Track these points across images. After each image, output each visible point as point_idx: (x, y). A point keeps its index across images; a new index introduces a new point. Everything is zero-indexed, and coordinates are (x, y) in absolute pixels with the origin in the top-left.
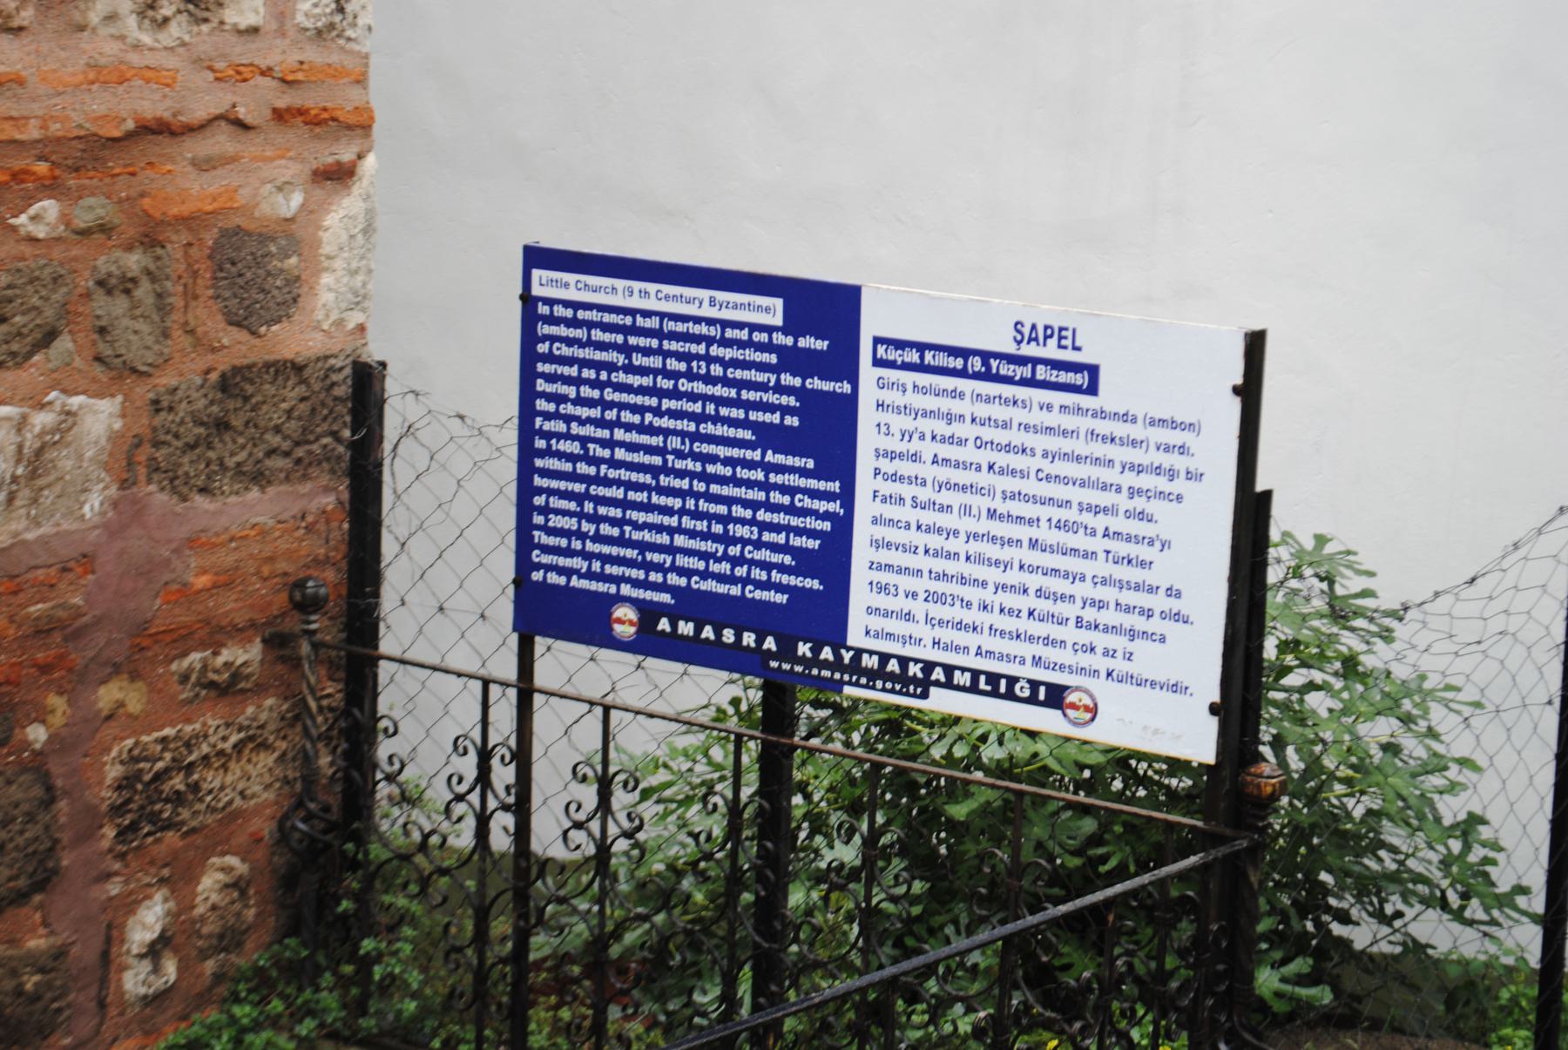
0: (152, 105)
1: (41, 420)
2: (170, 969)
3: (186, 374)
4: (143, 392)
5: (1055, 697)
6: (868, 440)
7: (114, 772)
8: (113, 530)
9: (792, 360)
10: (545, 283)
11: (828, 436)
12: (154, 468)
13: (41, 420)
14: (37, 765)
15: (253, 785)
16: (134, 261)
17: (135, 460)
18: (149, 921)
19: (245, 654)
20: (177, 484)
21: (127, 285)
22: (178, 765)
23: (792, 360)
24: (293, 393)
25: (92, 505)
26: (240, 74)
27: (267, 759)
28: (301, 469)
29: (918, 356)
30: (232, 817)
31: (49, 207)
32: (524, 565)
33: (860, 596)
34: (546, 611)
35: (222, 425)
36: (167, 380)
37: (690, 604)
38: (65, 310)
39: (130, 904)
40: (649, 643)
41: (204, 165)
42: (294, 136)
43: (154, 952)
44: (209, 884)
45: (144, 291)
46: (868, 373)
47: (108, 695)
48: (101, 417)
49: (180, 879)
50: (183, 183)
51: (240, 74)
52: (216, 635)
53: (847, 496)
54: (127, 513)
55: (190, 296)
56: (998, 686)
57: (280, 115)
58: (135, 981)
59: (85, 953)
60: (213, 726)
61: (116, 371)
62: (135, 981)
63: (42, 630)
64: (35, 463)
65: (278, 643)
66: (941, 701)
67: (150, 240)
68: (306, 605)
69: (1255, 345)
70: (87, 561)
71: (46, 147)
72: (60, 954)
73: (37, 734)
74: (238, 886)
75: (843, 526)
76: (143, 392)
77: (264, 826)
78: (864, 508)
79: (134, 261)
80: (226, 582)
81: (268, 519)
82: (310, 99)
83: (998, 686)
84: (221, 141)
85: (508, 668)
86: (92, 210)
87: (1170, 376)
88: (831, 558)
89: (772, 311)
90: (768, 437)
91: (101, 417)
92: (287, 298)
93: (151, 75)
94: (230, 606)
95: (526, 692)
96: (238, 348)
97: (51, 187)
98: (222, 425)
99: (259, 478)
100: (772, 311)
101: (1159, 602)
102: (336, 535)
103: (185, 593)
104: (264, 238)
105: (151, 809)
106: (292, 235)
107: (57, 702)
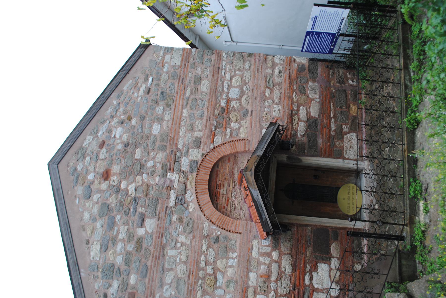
0: (288, 77)
1: (310, 89)
2: (355, 80)
3: (308, 75)
4: (309, 79)
5: (343, 20)
6: (319, 31)
7: (338, 84)
8: (319, 83)
9: (312, 35)
10: (304, 50)
11: (318, 34)
12: (315, 79)
13: (310, 89)
14: (336, 91)
15: (341, 71)
16: (299, 80)
17: (314, 81)
18: (350, 82)
19: (331, 71)
20: (317, 77)
21: (301, 80)
22: (339, 78)
23: (312, 35)
24: (311, 66)
25: (317, 85)
26: (286, 69)
27: (340, 70)
28: (317, 65)
29: (313, 27)
30: (344, 74)
31: (294, 86)
32: (326, 53)
33: (332, 32)
34: (331, 52)
35: (313, 72)
36: (308, 77)
37: (331, 43)
38: (302, 86)
39: (349, 83)
40: (334, 46)
41: (292, 73)
42: (291, 64)
43: (353, 81)
44: (349, 76)
45: (301, 79)
46: (314, 31)
47: (332, 84)
48: (310, 83)
49: (348, 79)
50: (294, 75)
51: (286, 69)
52: (329, 74)
53: (324, 33)
54: (318, 82)
55: (302, 75)
56: (341, 24)
57: (289, 65)
58: (355, 83)
59: (352, 88)
60: (336, 75)
61: (307, 82)
62: (355, 83)
63: (326, 90)
64: (313, 89)
65: (330, 69)
66: (342, 27)
67: (297, 78)
68: (328, 67)
69: (315, 5)
70: (321, 85)
71: (290, 86)
72: (351, 90)
73: (334, 91)
74: (349, 73)
75: (327, 33)
76: (309, 79)
77: (345, 71)
78: (325, 31)
79: (299, 80)
80: (325, 73)
81: (320, 69)
82: (288, 62)
83: (341, 24)
84: (291, 71)
85: (335, 55)
86: (295, 83)
87: (317, 11)
88: (329, 34)
89: (308, 37)
90: (318, 37)
91: (310, 83)
92: (303, 65)
93: (285, 77)
94: (327, 73)
95: (337, 53)
96: (307, 71)
97: (293, 86)
98: (313, 72)
99: (317, 69)
100: (308, 37)
101: (336, 12)
102: (317, 109)
103: (325, 77)
104: (298, 67)
105: (342, 81)
106: (299, 65)
107: (332, 89)
